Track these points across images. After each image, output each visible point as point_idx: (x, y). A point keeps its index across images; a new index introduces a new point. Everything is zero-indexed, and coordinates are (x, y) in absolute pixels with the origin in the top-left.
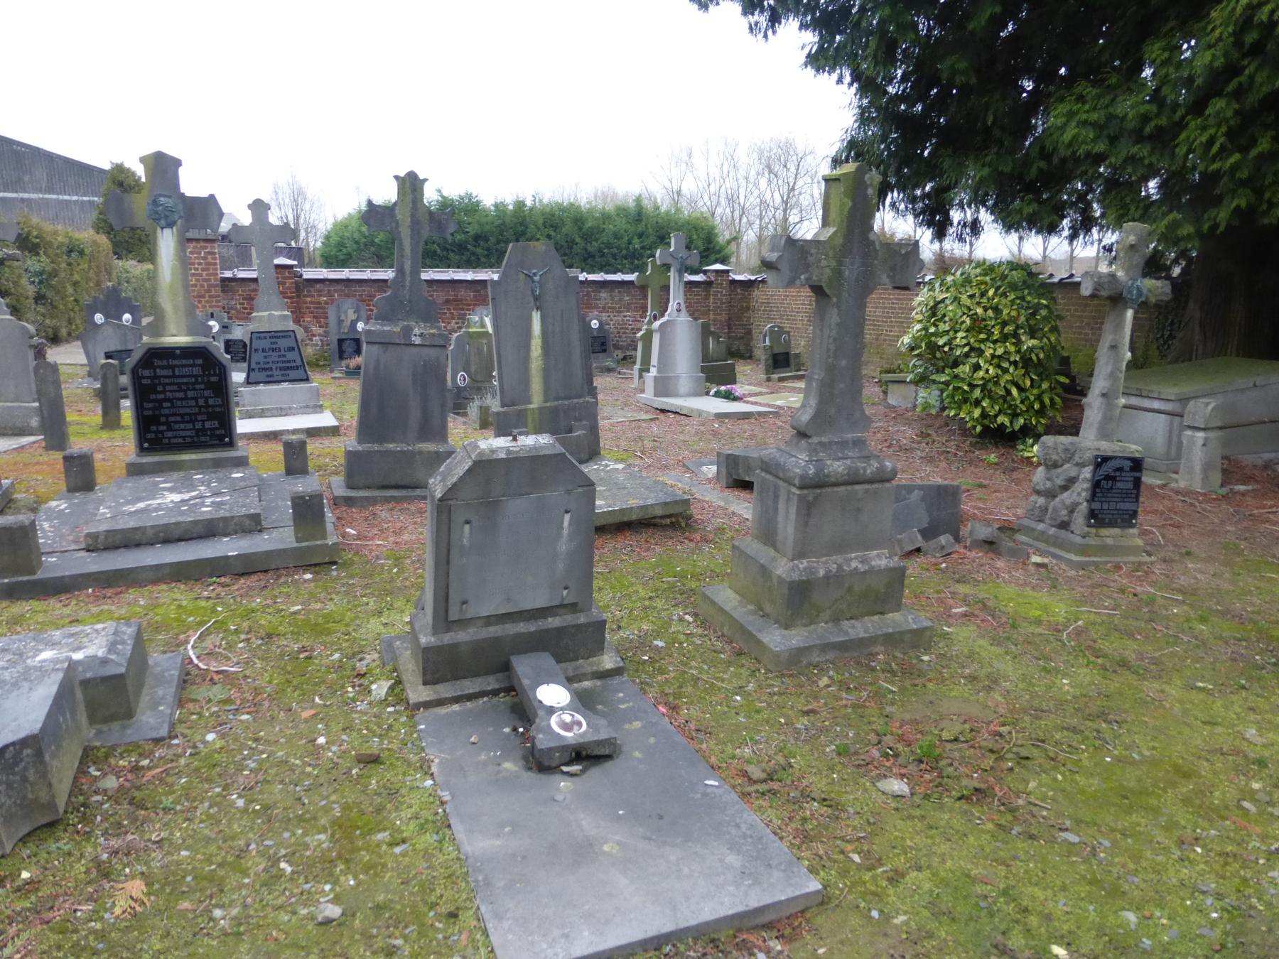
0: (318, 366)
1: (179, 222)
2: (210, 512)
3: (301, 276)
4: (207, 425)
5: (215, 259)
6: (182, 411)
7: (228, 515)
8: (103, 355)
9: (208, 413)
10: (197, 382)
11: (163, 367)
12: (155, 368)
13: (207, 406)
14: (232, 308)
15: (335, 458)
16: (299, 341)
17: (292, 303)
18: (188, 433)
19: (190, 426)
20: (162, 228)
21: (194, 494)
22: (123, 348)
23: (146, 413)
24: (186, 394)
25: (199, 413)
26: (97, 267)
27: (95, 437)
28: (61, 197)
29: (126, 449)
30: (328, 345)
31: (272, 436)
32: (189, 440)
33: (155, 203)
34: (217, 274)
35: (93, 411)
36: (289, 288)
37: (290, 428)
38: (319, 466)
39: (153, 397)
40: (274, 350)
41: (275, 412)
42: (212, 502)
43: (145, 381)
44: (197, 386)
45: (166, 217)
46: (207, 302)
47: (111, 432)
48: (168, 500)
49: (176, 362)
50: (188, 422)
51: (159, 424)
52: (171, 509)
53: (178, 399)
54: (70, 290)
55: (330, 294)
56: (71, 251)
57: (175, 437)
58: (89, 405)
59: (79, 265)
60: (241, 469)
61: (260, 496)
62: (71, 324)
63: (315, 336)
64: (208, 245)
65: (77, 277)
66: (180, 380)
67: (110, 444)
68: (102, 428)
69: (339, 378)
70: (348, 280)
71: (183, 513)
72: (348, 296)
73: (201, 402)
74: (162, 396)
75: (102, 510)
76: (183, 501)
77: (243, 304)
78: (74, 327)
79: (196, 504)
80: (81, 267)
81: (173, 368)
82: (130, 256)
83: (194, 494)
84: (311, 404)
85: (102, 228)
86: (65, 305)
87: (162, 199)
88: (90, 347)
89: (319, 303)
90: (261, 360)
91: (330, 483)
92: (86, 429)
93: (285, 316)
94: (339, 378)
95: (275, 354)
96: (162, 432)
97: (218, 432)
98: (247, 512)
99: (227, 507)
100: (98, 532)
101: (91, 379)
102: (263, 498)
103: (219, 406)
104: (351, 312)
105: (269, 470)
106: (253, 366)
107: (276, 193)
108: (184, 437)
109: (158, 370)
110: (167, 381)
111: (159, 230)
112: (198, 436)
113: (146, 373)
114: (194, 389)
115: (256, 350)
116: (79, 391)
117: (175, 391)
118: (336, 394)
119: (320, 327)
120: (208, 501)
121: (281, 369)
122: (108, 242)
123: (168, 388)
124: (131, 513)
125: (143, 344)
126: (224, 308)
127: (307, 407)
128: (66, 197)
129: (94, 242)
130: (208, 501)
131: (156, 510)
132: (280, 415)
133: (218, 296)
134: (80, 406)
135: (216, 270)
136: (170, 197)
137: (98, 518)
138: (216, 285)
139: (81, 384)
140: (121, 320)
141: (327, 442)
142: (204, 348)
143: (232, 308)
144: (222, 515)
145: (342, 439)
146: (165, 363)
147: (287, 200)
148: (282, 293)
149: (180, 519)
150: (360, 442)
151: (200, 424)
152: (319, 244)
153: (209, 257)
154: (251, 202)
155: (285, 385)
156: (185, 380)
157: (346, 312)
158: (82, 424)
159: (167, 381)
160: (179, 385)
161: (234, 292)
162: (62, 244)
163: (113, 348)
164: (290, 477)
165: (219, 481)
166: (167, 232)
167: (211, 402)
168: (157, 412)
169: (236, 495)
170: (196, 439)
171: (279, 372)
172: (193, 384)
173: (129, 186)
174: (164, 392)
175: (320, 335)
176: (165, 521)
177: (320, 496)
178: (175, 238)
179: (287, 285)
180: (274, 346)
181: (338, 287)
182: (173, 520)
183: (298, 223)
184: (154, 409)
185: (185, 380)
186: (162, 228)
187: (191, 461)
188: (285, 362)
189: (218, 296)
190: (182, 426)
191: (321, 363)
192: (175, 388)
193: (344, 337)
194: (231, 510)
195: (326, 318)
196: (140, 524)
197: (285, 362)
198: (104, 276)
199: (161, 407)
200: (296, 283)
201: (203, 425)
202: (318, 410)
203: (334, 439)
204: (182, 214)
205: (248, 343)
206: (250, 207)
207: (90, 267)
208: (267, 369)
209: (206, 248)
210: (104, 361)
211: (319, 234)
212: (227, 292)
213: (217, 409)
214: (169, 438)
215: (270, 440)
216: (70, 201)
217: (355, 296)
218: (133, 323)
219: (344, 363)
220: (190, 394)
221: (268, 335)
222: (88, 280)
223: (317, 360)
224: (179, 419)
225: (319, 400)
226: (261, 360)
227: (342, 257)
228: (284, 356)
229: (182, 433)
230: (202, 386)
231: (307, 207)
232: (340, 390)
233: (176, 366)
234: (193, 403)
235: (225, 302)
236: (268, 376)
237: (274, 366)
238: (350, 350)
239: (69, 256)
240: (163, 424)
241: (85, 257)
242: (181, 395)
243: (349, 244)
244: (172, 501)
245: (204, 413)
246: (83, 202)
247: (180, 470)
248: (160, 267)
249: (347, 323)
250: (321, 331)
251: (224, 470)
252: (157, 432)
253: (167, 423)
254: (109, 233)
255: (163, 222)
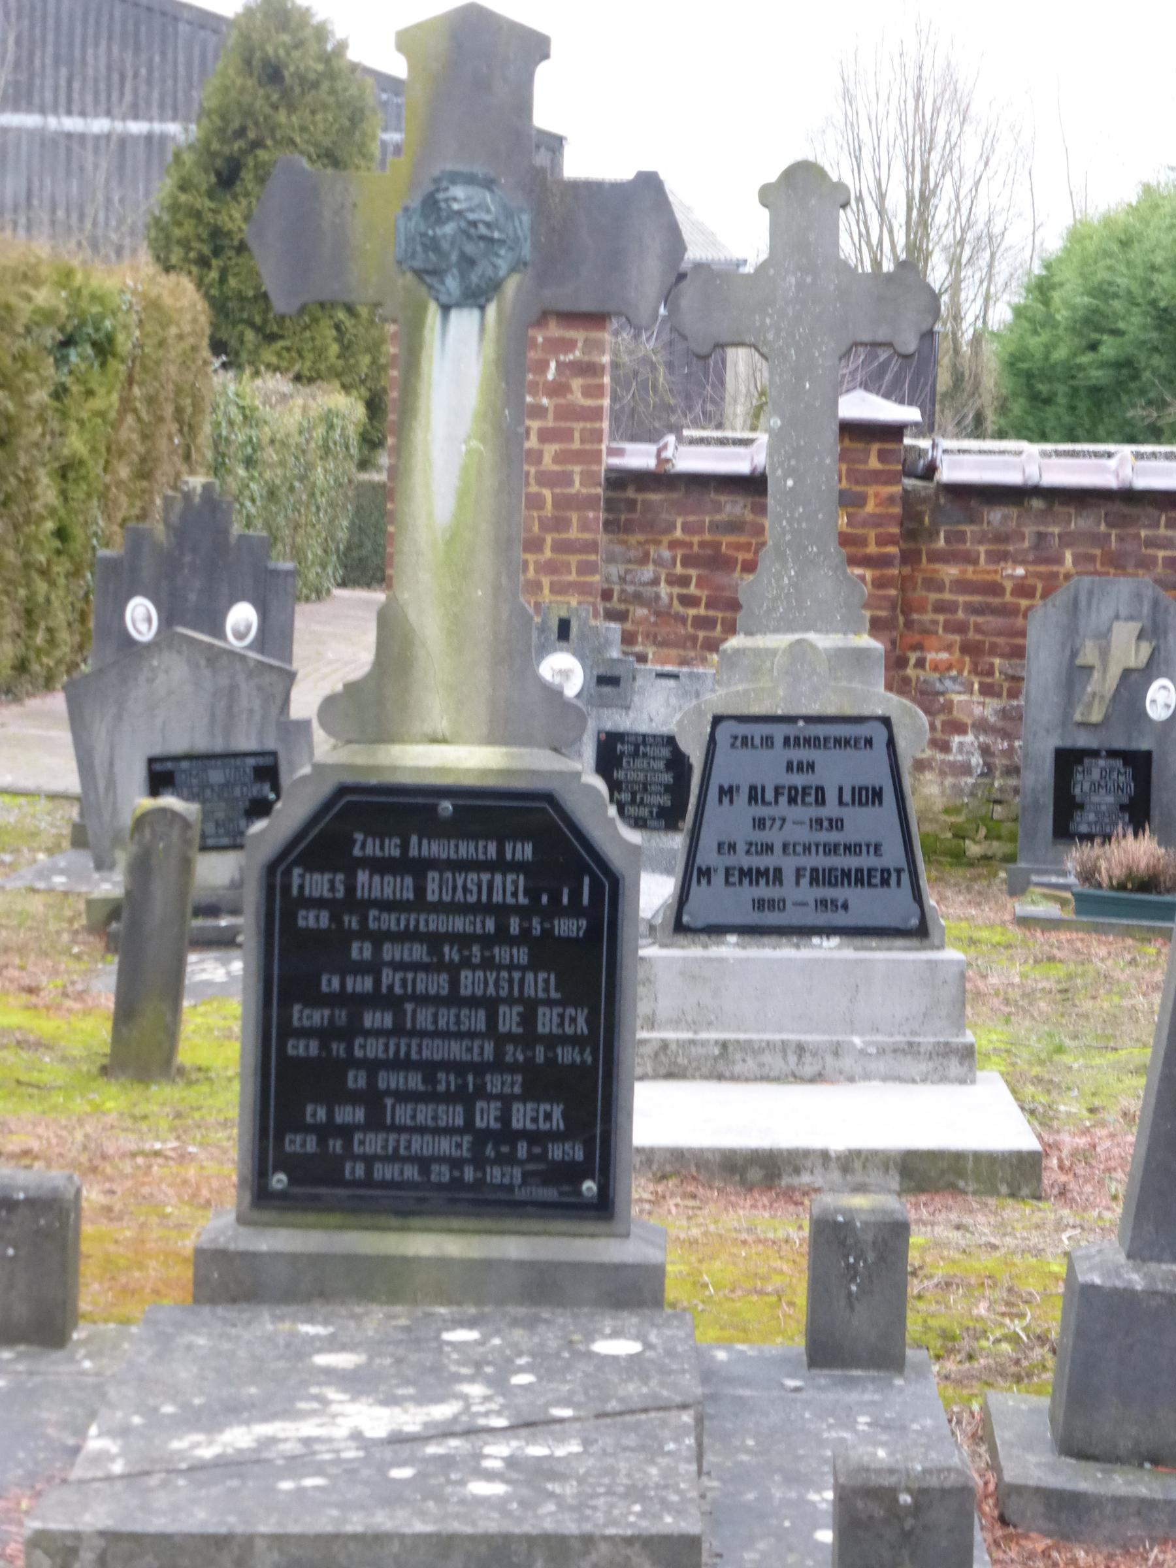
0: (958, 857)
1: (511, 286)
2: (499, 1505)
3: (930, 470)
4: (522, 1116)
5: (598, 391)
6: (434, 1050)
7: (571, 1526)
8: (138, 774)
9: (528, 1068)
10: (502, 936)
11: (381, 866)
12: (350, 867)
13: (529, 1037)
14: (638, 598)
15: (1014, 1304)
16: (906, 765)
17: (879, 584)
18: (445, 1146)
19: (455, 1116)
20: (446, 309)
21: (443, 1411)
22: (219, 746)
23: (297, 1048)
24: (454, 984)
25: (499, 1065)
26: (151, 400)
27: (79, 1105)
28: (53, 123)
29: (191, 1172)
30: (1013, 771)
31: (755, 1174)
32: (441, 1173)
33: (432, 207)
34: (596, 456)
35: (80, 996)
36: (877, 521)
37: (838, 1142)
38: (946, 1336)
39: (330, 983)
40: (795, 796)
41: (774, 1062)
42: (512, 1462)
43: (308, 919)
44: (502, 954)
45: (468, 262)
46: (550, 568)
47: (136, 1092)
48: (341, 1430)
49: (435, 849)
50: (448, 1098)
51: (338, 1095)
52: (350, 1471)
53: (424, 1000)
54: (47, 491)
55: (1043, 552)
56: (68, 342)
57: (395, 1158)
58: (65, 963)
59: (90, 393)
60: (632, 1320)
61: (700, 1457)
62: (31, 625)
63: (960, 729)
64: (578, 335)
65: (75, 444)
66: (436, 923)
67: (129, 1142)
68: (104, 1071)
69: (1049, 924)
70: (1129, 497)
71: (393, 1496)
72: (1116, 562)
73: (509, 1020)
74: (365, 984)
75: (95, 1442)
76: (398, 1439)
77: (684, 581)
78: (40, 638)
79: (447, 1462)
80: (97, 403)
81: (419, 868)
82: (268, 355)
83: (443, 1411)
84: (927, 1040)
85: (185, 244)
86: (24, 551)
87: (459, 191)
88: (100, 732)
89: (995, 589)
90: (742, 832)
91: (986, 1419)
92: (51, 1071)
93: (860, 655)
94: (1049, 924)
95: (806, 812)
96: (346, 1132)
97: (556, 1152)
98: (648, 1527)
99: (569, 1490)
100: (77, 1535)
101: (84, 859)
102: (710, 1458)
103: (575, 1041)
104: (1124, 634)
105: (744, 1331)
106: (707, 856)
107: (848, 96)
108: (424, 1164)
109: (362, 877)
110: (390, 922)
111: (433, 313)
112: (479, 1162)
113: (318, 884)
114: (488, 964)
115: (727, 793)
116: (36, 905)
117: (416, 967)
118: (1029, 995)
119: (987, 690)
120: (497, 1452)
121: (817, 876)
122: (201, 305)
123: (390, 952)
124: (199, 1467)
125: (319, 768)
126: (607, 595)
127: (910, 1049)
128: (72, 124)
129: (154, 305)
130: (497, 1452)
131: (297, 1464)
132: (796, 1078)
133: (591, 547)
134: (37, 971)
135: (597, 436)
136: (488, 184)
137: (76, 1473)
138: (589, 502)
139: (45, 873)
140: (217, 629)
141: (983, 1224)
142: (549, 798)
143: (638, 598)
144: (549, 1526)
145: (1049, 1211)
146: (392, 848)
147: (890, 128)
148: (845, 540)
149: (383, 1520)
150: (1137, 1253)
151: (494, 1108)
152: (1001, 315)
153: (577, 384)
154: (773, 176)
155: (828, 947)
156: (459, 924)
157: (1104, 636)
158: (38, 1045)
159: (390, 922)
160: (434, 941)
161: (654, 528)
162: (48, 316)
163: (178, 744)
164: (823, 1376)
165: (543, 1363)
166: (464, 322)
167: (547, 1021)
168: (338, 1049)
169: (606, 1441)
170: (469, 1174)
171: (808, 893)
172: (487, 941)
173: (302, 79)
174: (373, 968)
175: (981, 726)
176: (323, 1522)
177: (964, 1493)
178: (490, 350)
179: (870, 507)
180: (799, 780)
181: (1081, 523)
182: (356, 1524)
183: (924, 224)
184: (325, 1035)
185: (459, 924)
186: (446, 309)
187: (443, 1263)
188: (831, 849)
189: (591, 547)
190: (424, 1114)
191: (974, 849)
192: (418, 952)
193: (1083, 740)
194: (580, 1507)
195: (1018, 652)
196: (231, 1523)
197: (831, 849)
198: (169, 438)
199: (354, 1030)
200: (907, 498)
201: (505, 1118)
202: (954, 1067)
203: (1018, 1213)
204: (526, 251)
205: (696, 757)
206: (767, 195)
207: (126, 404)
208: (762, 873)
209: (570, 345)
210: (147, 803)
211: (1002, 270)
212: (628, 528)
213: (566, 1055)
214: (369, 1161)
215: (749, 1187)
216: (82, 137)
217: (1146, 563)
218: (262, 643)
219: (1075, 857)
220: (471, 984)
221: (779, 732)
222: (114, 451)
223: (960, 834)
224: (415, 1081)
225: (959, 1023)
226: (742, 832)
227: (1098, 376)
228: (837, 824)
229: (421, 1145)
230: (521, 955)
231: (969, 155)
232: (1047, 978)
233: (432, 864)
234: (478, 1020)
235: (615, 570)
236: (760, 905)
237: (789, 865)
238: (1106, 800)
239: (61, 361)
240: (354, 1098)
241: (113, 364)
242: (438, 984)
243: (1135, 324)
244: (357, 1436)
245: (513, 1068)
246: (124, 141)
247: (394, 1296)
248: (418, 462)
249: (1104, 683)
250: (988, 709)
251: (563, 1318)
252: (325, 1131)
253: (372, 1099)
254: (203, 263)
255: (452, 283)
